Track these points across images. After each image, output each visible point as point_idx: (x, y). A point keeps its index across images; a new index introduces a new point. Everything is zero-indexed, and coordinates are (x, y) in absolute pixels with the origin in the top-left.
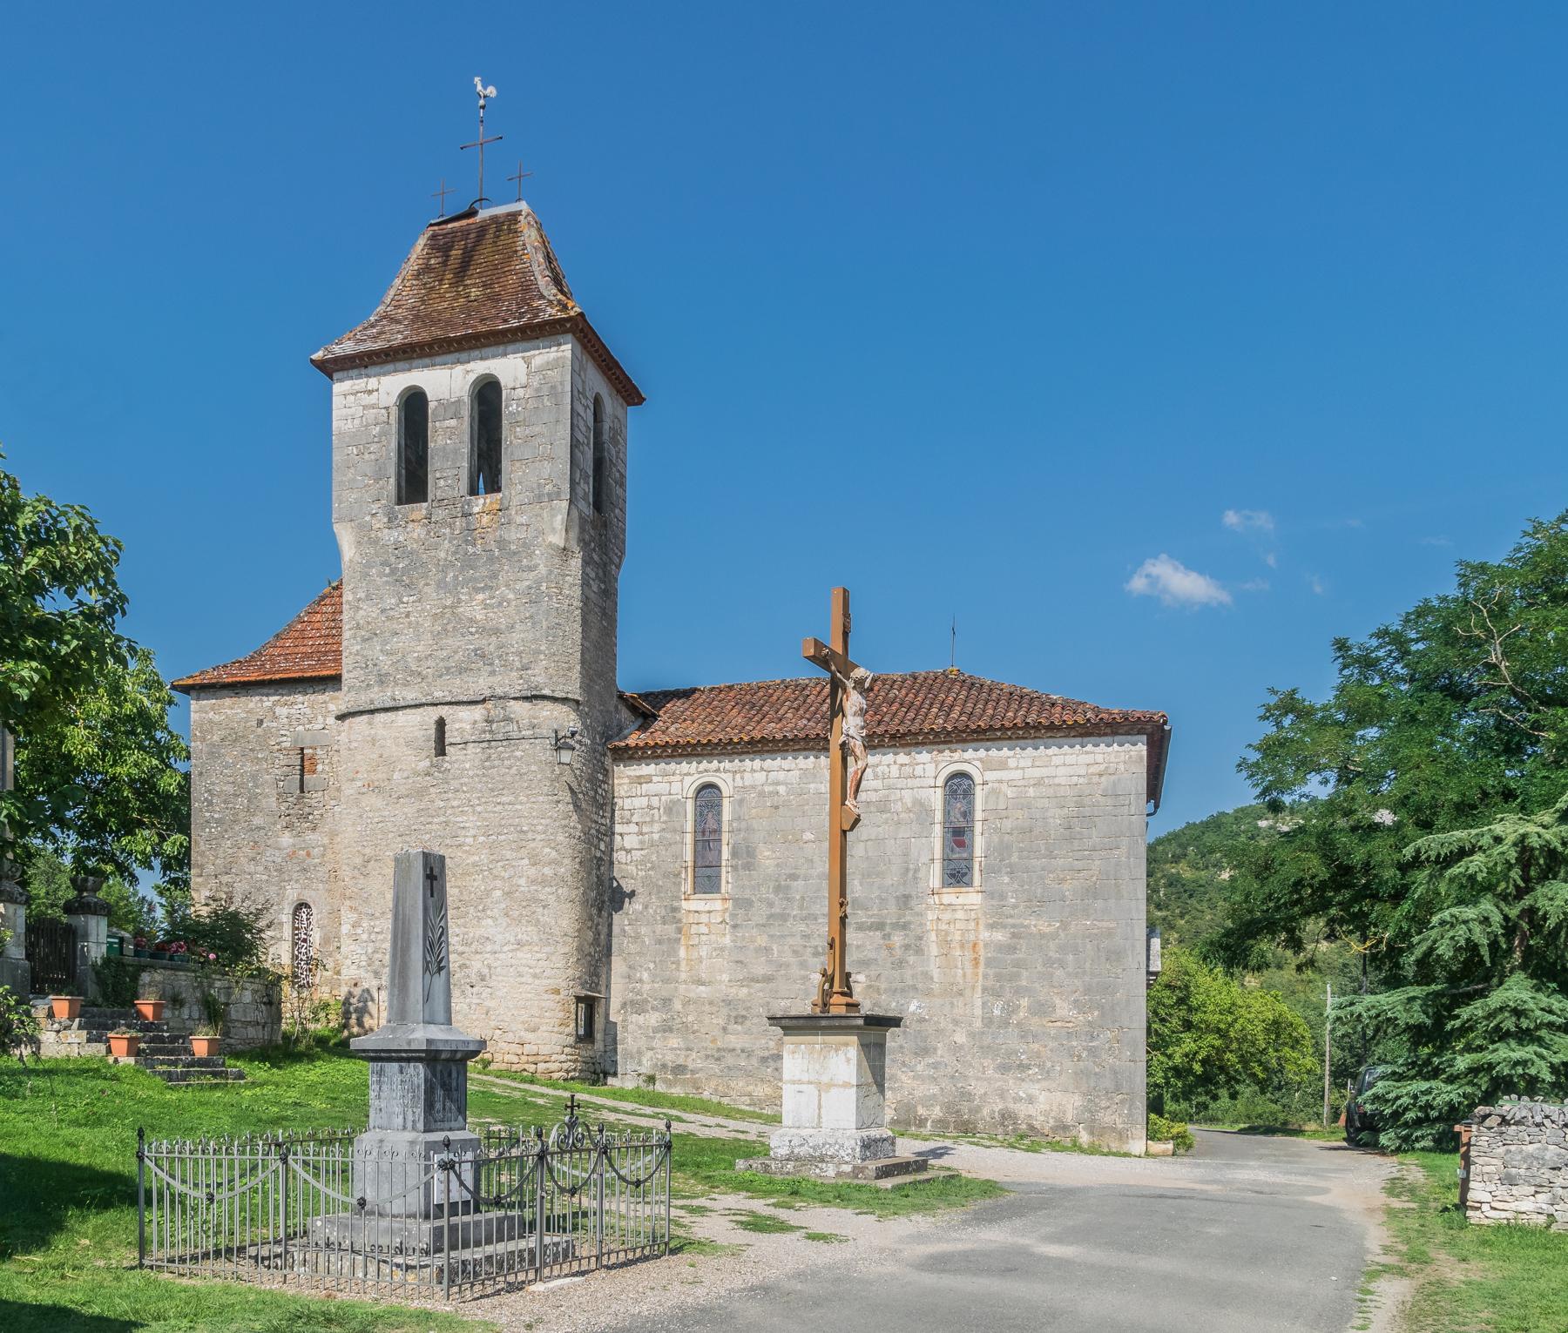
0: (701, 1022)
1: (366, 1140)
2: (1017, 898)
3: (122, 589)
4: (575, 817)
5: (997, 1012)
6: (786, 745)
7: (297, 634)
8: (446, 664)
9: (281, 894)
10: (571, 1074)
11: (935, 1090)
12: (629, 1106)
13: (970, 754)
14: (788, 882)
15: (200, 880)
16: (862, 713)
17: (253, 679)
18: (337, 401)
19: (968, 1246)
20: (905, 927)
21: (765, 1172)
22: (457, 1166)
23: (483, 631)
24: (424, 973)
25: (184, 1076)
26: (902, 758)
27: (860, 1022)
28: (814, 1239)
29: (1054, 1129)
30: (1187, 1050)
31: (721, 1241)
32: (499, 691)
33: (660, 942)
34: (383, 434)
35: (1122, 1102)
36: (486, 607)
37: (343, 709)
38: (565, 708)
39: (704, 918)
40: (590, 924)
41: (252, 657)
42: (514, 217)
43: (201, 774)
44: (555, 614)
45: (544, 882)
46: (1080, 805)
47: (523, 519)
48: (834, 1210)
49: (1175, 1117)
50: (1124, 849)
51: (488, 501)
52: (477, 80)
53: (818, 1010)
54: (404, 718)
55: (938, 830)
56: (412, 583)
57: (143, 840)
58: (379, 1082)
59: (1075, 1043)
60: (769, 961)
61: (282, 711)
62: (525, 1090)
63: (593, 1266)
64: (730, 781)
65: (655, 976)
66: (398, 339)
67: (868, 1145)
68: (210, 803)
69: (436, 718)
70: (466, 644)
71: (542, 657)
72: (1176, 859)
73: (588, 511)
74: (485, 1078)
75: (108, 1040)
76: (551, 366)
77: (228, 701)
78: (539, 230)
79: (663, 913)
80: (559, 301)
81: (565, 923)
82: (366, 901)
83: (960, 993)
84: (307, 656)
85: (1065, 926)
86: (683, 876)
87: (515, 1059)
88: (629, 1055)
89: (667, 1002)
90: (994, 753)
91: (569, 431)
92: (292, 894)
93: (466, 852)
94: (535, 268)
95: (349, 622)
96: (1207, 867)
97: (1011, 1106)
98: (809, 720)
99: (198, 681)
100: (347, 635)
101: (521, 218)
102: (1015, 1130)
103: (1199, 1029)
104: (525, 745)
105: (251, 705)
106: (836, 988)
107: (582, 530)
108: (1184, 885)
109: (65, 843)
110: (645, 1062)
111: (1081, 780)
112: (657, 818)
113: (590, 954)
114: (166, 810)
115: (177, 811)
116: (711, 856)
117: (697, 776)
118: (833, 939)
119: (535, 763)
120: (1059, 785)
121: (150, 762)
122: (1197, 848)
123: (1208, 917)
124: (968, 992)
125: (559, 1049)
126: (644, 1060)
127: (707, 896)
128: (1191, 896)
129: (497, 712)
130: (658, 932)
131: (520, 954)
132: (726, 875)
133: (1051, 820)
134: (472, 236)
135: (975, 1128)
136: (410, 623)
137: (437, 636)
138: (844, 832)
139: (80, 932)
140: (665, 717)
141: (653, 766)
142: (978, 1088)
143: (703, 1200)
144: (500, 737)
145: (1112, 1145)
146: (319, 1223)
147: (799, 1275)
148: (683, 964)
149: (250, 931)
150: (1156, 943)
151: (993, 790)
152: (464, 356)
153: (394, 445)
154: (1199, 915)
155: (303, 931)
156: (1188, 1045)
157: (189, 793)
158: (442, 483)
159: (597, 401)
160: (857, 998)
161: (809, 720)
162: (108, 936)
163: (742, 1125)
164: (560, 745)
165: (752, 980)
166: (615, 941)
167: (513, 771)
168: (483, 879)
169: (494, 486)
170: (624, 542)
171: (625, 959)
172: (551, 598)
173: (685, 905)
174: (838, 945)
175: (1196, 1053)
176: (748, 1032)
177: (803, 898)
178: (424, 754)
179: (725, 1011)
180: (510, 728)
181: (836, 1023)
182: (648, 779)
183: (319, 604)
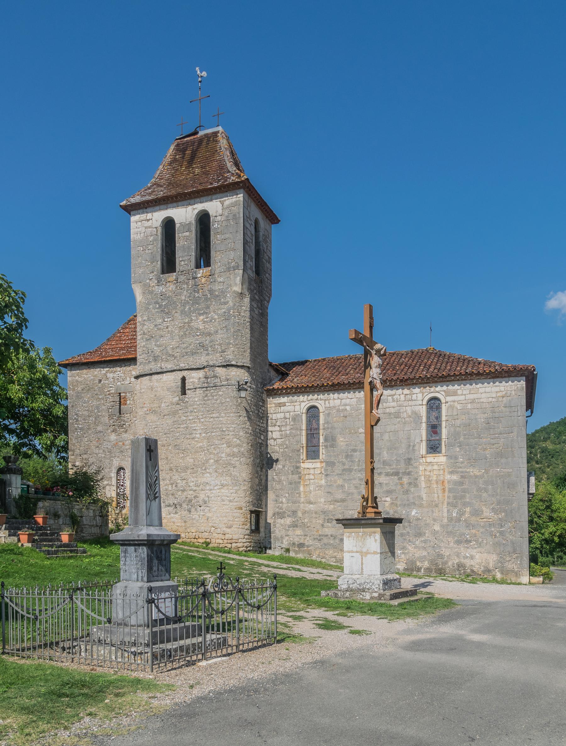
0: (311, 522)
1: (118, 589)
2: (463, 459)
3: (26, 316)
4: (248, 423)
5: (454, 515)
6: (350, 386)
8: (186, 351)
9: (111, 464)
10: (249, 548)
11: (425, 553)
12: (275, 564)
13: (439, 388)
15: (73, 457)
16: (380, 366)
17: (96, 360)
18: (133, 225)
19: (433, 636)
20: (409, 474)
21: (336, 597)
22: (156, 601)
23: (203, 334)
24: (147, 500)
25: (56, 552)
26: (406, 391)
27: (381, 521)
28: (353, 634)
29: (484, 572)
30: (551, 530)
31: (306, 635)
32: (211, 363)
33: (291, 484)
34: (155, 240)
35: (517, 557)
36: (204, 322)
37: (138, 374)
38: (243, 371)
39: (312, 471)
40: (256, 475)
41: (96, 350)
42: (215, 134)
43: (73, 406)
44: (237, 325)
45: (234, 455)
46: (493, 412)
47: (221, 279)
48: (367, 617)
49: (544, 565)
50: (515, 433)
51: (204, 271)
52: (197, 68)
53: (360, 515)
55: (424, 425)
57: (47, 437)
58: (125, 557)
59: (493, 529)
61: (110, 375)
62: (225, 557)
63: (234, 651)
64: (323, 404)
65: (289, 500)
66: (161, 194)
67: (386, 583)
68: (77, 420)
69: (181, 377)
71: (231, 346)
72: (545, 440)
73: (253, 275)
74: (206, 551)
75: (19, 535)
77: (85, 371)
78: (228, 140)
79: (292, 469)
80: (237, 173)
83: (437, 506)
84: (122, 349)
85: (487, 471)
87: (221, 542)
88: (277, 539)
89: (294, 512)
90: (450, 387)
91: (242, 236)
92: (116, 463)
93: (197, 441)
94: (226, 158)
95: (139, 332)
96: (560, 443)
97: (462, 560)
98: (361, 374)
99: (71, 361)
100: (139, 337)
101: (219, 134)
102: (464, 572)
103: (557, 520)
104: (224, 389)
105: (96, 373)
106: (370, 504)
107: (250, 284)
108: (549, 452)
109: (10, 440)
110: (284, 542)
111: (494, 400)
112: (288, 423)
113: (257, 490)
114: (57, 424)
115: (62, 425)
116: (315, 441)
117: (308, 402)
118: (367, 480)
119: (228, 397)
120: (483, 402)
121: (49, 401)
122: (555, 434)
123: (561, 467)
124: (440, 505)
125: (242, 536)
128: (552, 457)
129: (210, 373)
131: (223, 491)
132: (322, 450)
133: (479, 420)
134: (196, 144)
135: (445, 572)
136: (168, 331)
137: (181, 337)
138: (372, 426)
139: (7, 483)
140: (292, 374)
141: (286, 398)
142: (446, 552)
143: (302, 612)
144: (212, 385)
145: (512, 579)
146: (95, 630)
147: (342, 654)
148: (302, 494)
149: (93, 481)
150: (533, 479)
151: (451, 406)
152: (192, 201)
153: (159, 245)
154: (557, 466)
156: (552, 528)
157: (67, 415)
158: (183, 263)
159: (256, 222)
160: (380, 509)
161: (361, 374)
162: (22, 484)
164: (240, 388)
165: (336, 501)
166: (269, 483)
167: (218, 401)
168: (205, 455)
169: (208, 264)
170: (271, 290)
171: (274, 492)
173: (302, 465)
174: (370, 483)
175: (555, 532)
177: (359, 461)
178: (176, 394)
179: (322, 517)
181: (369, 522)
182: (284, 404)
183: (128, 324)
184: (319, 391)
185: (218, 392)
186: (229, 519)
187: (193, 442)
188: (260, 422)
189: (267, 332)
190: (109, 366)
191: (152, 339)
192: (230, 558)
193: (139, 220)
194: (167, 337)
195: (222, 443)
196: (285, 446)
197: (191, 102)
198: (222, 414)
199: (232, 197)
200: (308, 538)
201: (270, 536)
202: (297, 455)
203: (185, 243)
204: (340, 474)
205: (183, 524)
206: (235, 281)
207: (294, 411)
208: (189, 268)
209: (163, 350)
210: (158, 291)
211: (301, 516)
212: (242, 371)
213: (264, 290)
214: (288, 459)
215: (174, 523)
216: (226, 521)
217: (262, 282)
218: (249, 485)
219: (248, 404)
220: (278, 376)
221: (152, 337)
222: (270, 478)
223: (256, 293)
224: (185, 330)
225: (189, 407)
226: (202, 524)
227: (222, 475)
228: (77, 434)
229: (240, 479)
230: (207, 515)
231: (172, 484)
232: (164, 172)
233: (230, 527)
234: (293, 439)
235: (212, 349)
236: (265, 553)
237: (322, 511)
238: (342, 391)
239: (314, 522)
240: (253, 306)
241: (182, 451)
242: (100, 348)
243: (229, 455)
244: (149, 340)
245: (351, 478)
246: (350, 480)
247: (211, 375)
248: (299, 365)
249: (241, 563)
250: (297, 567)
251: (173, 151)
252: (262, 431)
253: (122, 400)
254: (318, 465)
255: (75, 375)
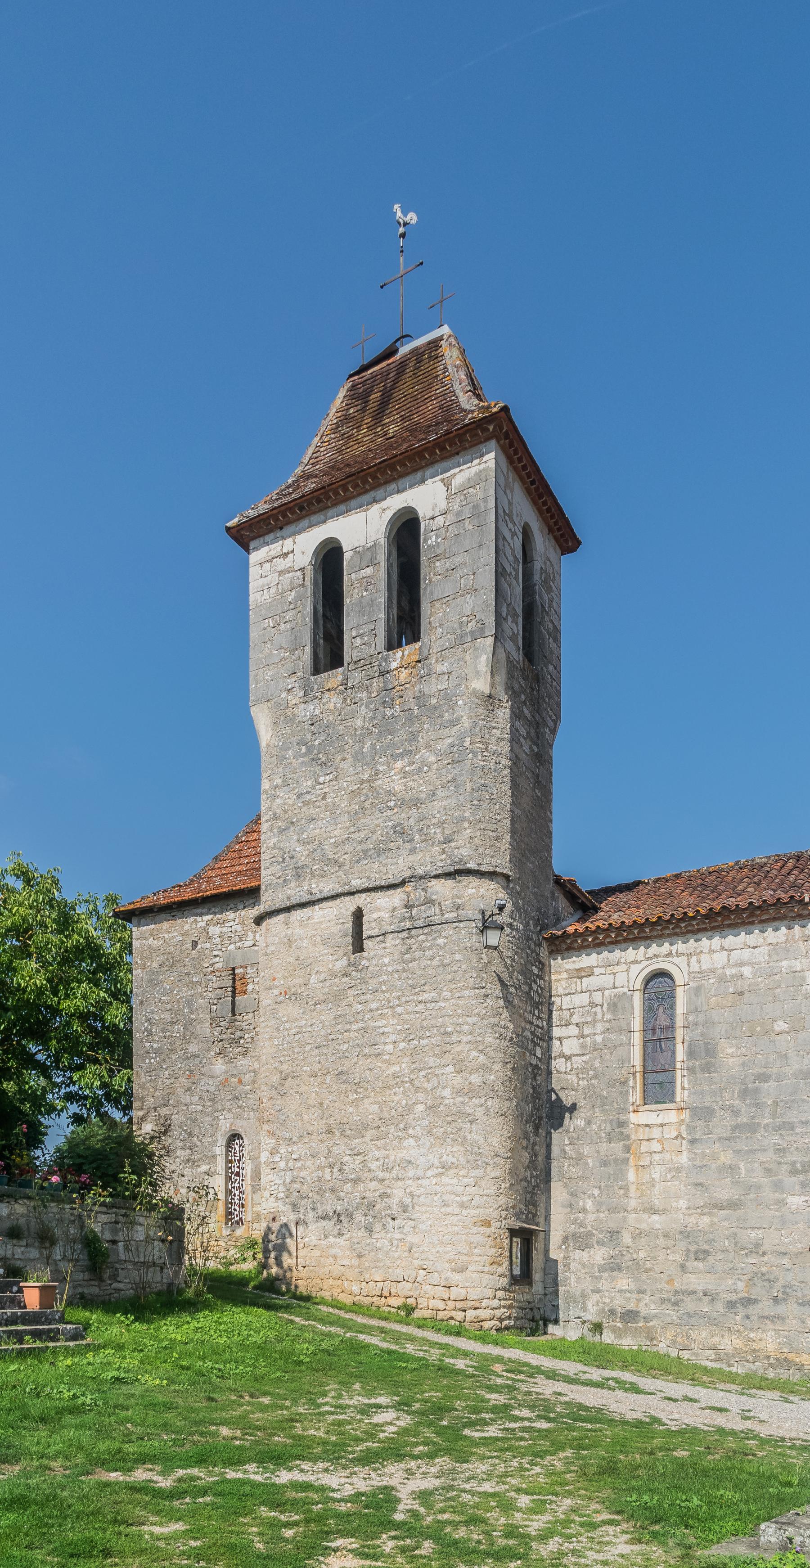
0: (654, 1258)
4: (506, 1015)
6: (752, 915)
7: (234, 855)
8: (364, 847)
9: (214, 1126)
12: (570, 1367)
14: (757, 1084)
18: (255, 581)
23: (405, 803)
32: (420, 871)
33: (605, 1164)
34: (300, 598)
36: (405, 775)
38: (493, 885)
39: (656, 1133)
40: (525, 1143)
41: (192, 881)
42: (435, 344)
44: (479, 772)
45: (470, 1092)
51: (406, 653)
52: (396, 207)
54: (321, 913)
56: (329, 760)
60: (736, 1183)
61: (215, 930)
62: (446, 1346)
64: (685, 969)
65: (600, 1204)
68: (150, 1033)
69: (352, 909)
70: (386, 821)
71: (466, 825)
73: (518, 656)
76: (472, 484)
77: (165, 925)
79: (609, 1128)
81: (495, 1141)
82: (283, 1124)
86: (631, 1083)
87: (441, 1305)
89: (614, 1234)
91: (493, 555)
92: (225, 1125)
93: (386, 1061)
94: (457, 387)
104: (449, 930)
105: (187, 927)
107: (510, 676)
110: (590, 1307)
112: (599, 1016)
113: (525, 1179)
116: (663, 1058)
117: (646, 963)
119: (460, 951)
121: (98, 995)
125: (490, 1293)
126: (589, 1305)
127: (659, 1106)
130: (603, 1153)
131: (445, 1180)
132: (681, 1080)
136: (326, 806)
137: (354, 816)
141: (594, 955)
144: (421, 923)
148: (633, 1188)
152: (380, 493)
153: (309, 608)
155: (236, 1164)
158: (358, 641)
163: (717, 1397)
166: (554, 1164)
167: (436, 962)
168: (404, 1092)
169: (415, 637)
170: (559, 705)
172: (475, 755)
173: (634, 1118)
176: (711, 1271)
177: (776, 1103)
178: (341, 952)
179: (682, 1245)
180: (431, 912)
182: (589, 972)
184: (676, 934)
185: (435, 939)
186: (460, 1249)
187: (379, 1064)
188: (534, 1015)
189: (550, 801)
190: (213, 909)
191: (292, 829)
192: (458, 1350)
193: (267, 558)
194: (323, 819)
195: (443, 1062)
196: (592, 1073)
197: (382, 287)
198: (445, 993)
199: (469, 465)
200: (647, 1299)
201: (556, 1293)
202: (621, 1092)
203: (365, 594)
204: (727, 1139)
205: (356, 1262)
206: (475, 667)
207: (614, 988)
208: (372, 651)
209: (315, 850)
210: (306, 715)
211: (631, 1244)
212: (492, 887)
213: (544, 701)
214: (598, 1103)
215: (335, 1257)
216: (451, 1255)
217: (538, 681)
218: (508, 1166)
219: (506, 967)
220: (575, 911)
221: (292, 823)
222: (555, 1150)
223: (524, 703)
224: (362, 799)
225: (370, 981)
226: (398, 1262)
227: (445, 1141)
228: (150, 1063)
229: (485, 1150)
230: (409, 1239)
231: (331, 1166)
232: (322, 449)
233: (462, 1270)
234: (611, 1054)
235: (423, 837)
236: (545, 1333)
237: (681, 1232)
238: (731, 931)
239: (662, 1257)
240: (517, 730)
241: (355, 1087)
242: (200, 877)
243: (459, 1092)
244: (284, 830)
245: (756, 1147)
246: (752, 1152)
247: (419, 899)
248: (621, 892)
249: (485, 1364)
250: (627, 1376)
251: (342, 402)
252: (538, 1038)
253: (238, 983)
254: (672, 1117)
255: (147, 935)
